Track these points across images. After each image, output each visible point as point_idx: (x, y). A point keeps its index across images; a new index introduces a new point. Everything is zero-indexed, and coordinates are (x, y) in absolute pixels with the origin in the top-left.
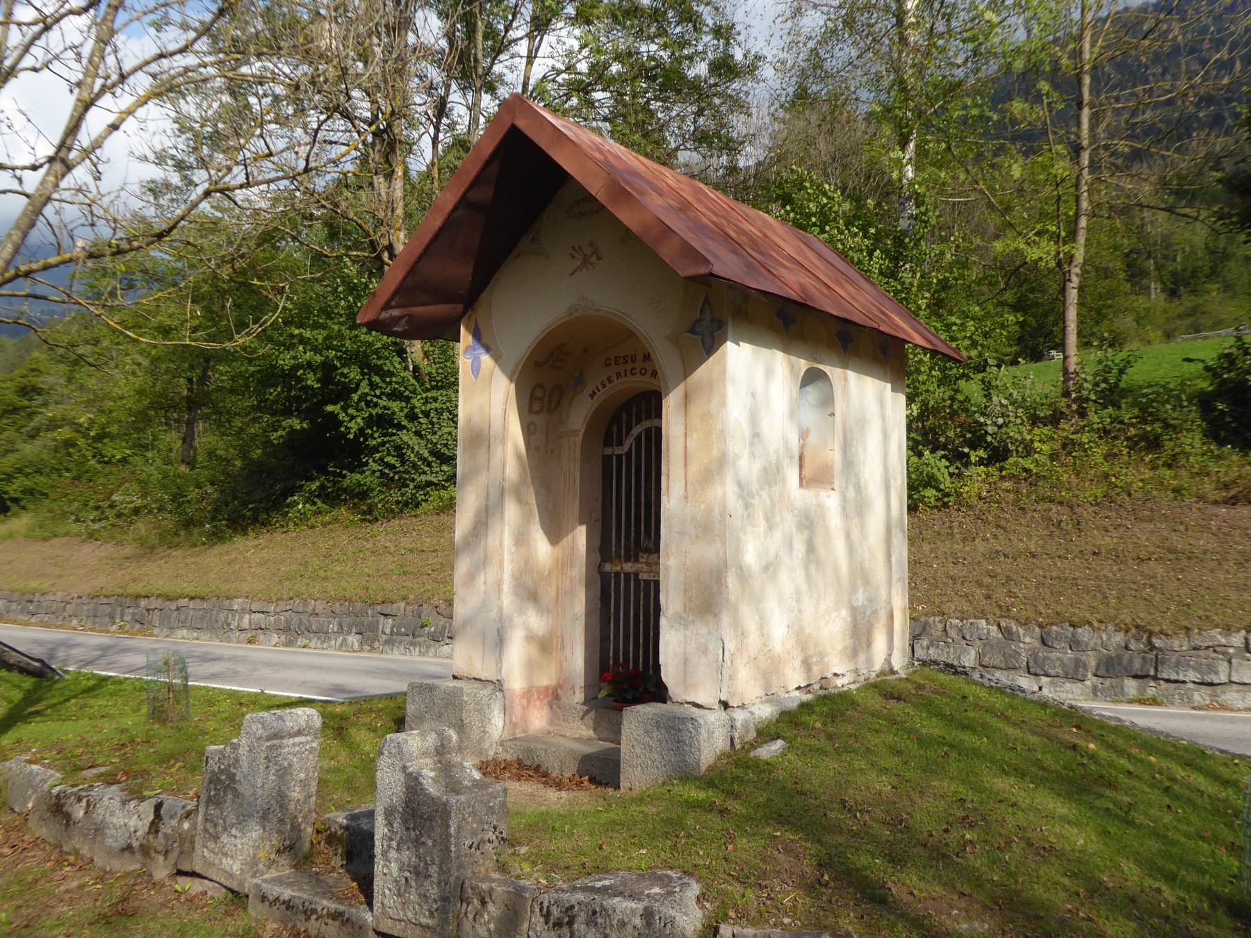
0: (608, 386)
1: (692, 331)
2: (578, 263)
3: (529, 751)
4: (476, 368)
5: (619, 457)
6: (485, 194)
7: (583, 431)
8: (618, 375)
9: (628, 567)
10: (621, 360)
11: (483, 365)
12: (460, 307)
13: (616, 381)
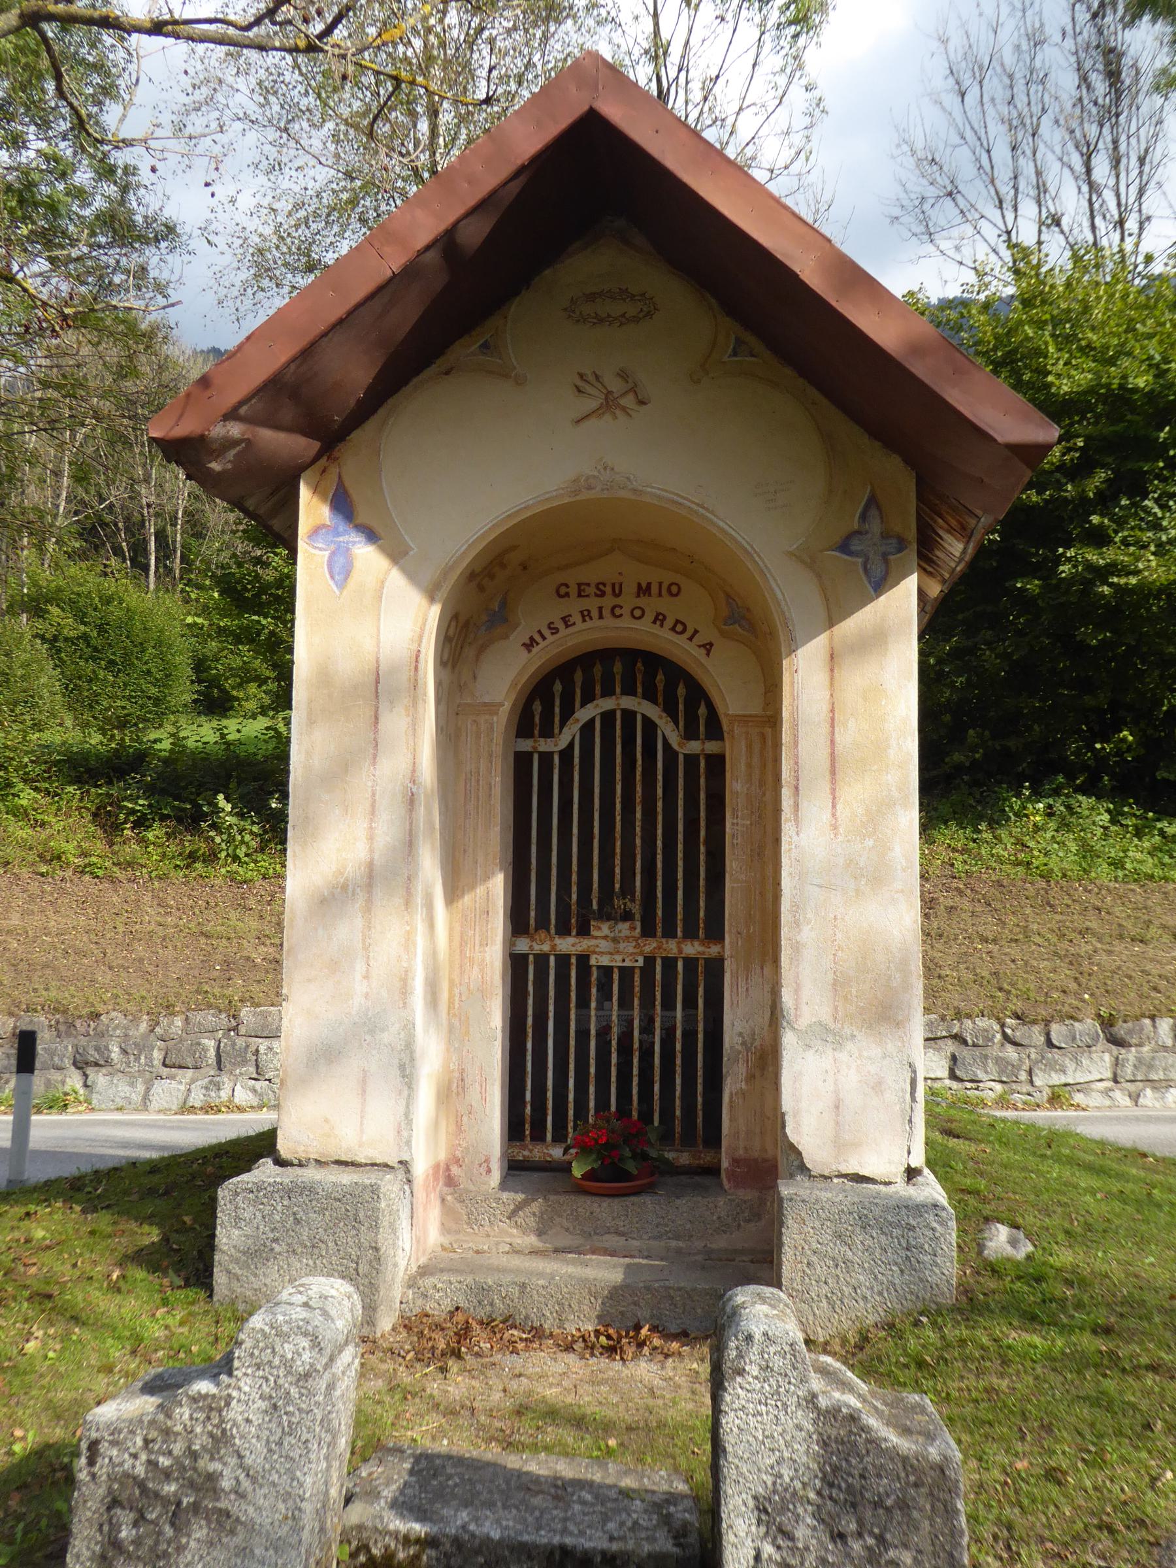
0: (563, 631)
1: (844, 547)
2: (593, 404)
3: (483, 1290)
4: (341, 571)
5: (546, 758)
6: (474, 235)
7: (507, 706)
8: (585, 615)
9: (568, 945)
10: (592, 590)
11: (358, 564)
12: (316, 445)
13: (580, 625)
